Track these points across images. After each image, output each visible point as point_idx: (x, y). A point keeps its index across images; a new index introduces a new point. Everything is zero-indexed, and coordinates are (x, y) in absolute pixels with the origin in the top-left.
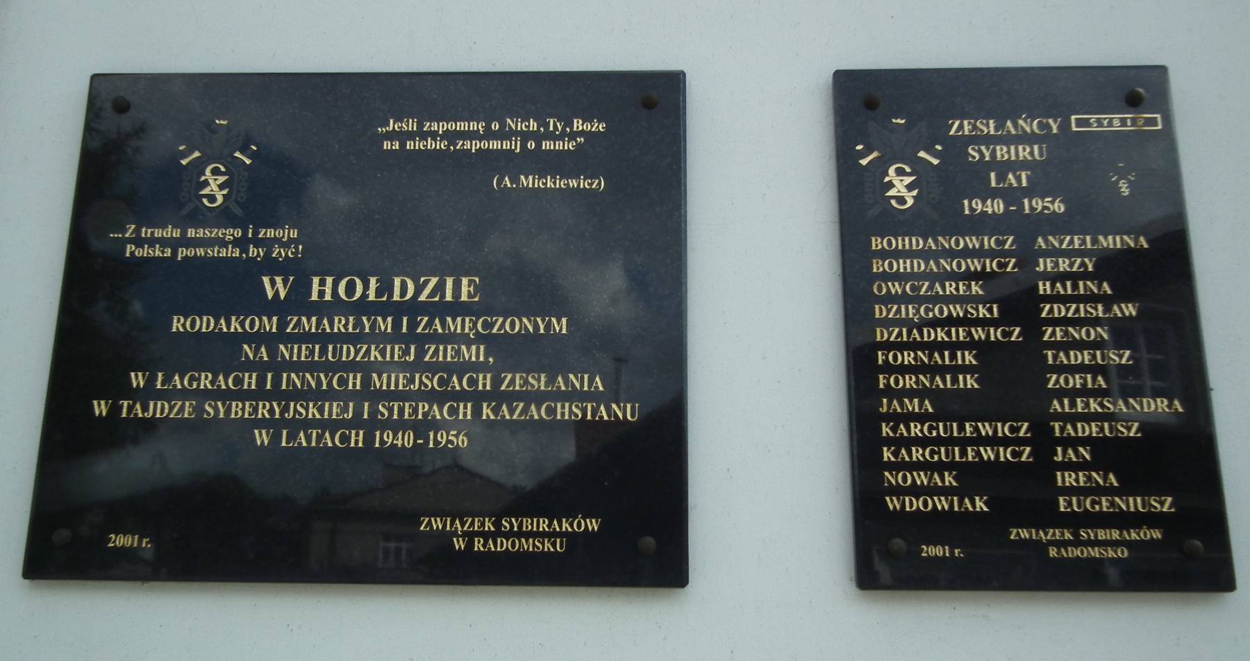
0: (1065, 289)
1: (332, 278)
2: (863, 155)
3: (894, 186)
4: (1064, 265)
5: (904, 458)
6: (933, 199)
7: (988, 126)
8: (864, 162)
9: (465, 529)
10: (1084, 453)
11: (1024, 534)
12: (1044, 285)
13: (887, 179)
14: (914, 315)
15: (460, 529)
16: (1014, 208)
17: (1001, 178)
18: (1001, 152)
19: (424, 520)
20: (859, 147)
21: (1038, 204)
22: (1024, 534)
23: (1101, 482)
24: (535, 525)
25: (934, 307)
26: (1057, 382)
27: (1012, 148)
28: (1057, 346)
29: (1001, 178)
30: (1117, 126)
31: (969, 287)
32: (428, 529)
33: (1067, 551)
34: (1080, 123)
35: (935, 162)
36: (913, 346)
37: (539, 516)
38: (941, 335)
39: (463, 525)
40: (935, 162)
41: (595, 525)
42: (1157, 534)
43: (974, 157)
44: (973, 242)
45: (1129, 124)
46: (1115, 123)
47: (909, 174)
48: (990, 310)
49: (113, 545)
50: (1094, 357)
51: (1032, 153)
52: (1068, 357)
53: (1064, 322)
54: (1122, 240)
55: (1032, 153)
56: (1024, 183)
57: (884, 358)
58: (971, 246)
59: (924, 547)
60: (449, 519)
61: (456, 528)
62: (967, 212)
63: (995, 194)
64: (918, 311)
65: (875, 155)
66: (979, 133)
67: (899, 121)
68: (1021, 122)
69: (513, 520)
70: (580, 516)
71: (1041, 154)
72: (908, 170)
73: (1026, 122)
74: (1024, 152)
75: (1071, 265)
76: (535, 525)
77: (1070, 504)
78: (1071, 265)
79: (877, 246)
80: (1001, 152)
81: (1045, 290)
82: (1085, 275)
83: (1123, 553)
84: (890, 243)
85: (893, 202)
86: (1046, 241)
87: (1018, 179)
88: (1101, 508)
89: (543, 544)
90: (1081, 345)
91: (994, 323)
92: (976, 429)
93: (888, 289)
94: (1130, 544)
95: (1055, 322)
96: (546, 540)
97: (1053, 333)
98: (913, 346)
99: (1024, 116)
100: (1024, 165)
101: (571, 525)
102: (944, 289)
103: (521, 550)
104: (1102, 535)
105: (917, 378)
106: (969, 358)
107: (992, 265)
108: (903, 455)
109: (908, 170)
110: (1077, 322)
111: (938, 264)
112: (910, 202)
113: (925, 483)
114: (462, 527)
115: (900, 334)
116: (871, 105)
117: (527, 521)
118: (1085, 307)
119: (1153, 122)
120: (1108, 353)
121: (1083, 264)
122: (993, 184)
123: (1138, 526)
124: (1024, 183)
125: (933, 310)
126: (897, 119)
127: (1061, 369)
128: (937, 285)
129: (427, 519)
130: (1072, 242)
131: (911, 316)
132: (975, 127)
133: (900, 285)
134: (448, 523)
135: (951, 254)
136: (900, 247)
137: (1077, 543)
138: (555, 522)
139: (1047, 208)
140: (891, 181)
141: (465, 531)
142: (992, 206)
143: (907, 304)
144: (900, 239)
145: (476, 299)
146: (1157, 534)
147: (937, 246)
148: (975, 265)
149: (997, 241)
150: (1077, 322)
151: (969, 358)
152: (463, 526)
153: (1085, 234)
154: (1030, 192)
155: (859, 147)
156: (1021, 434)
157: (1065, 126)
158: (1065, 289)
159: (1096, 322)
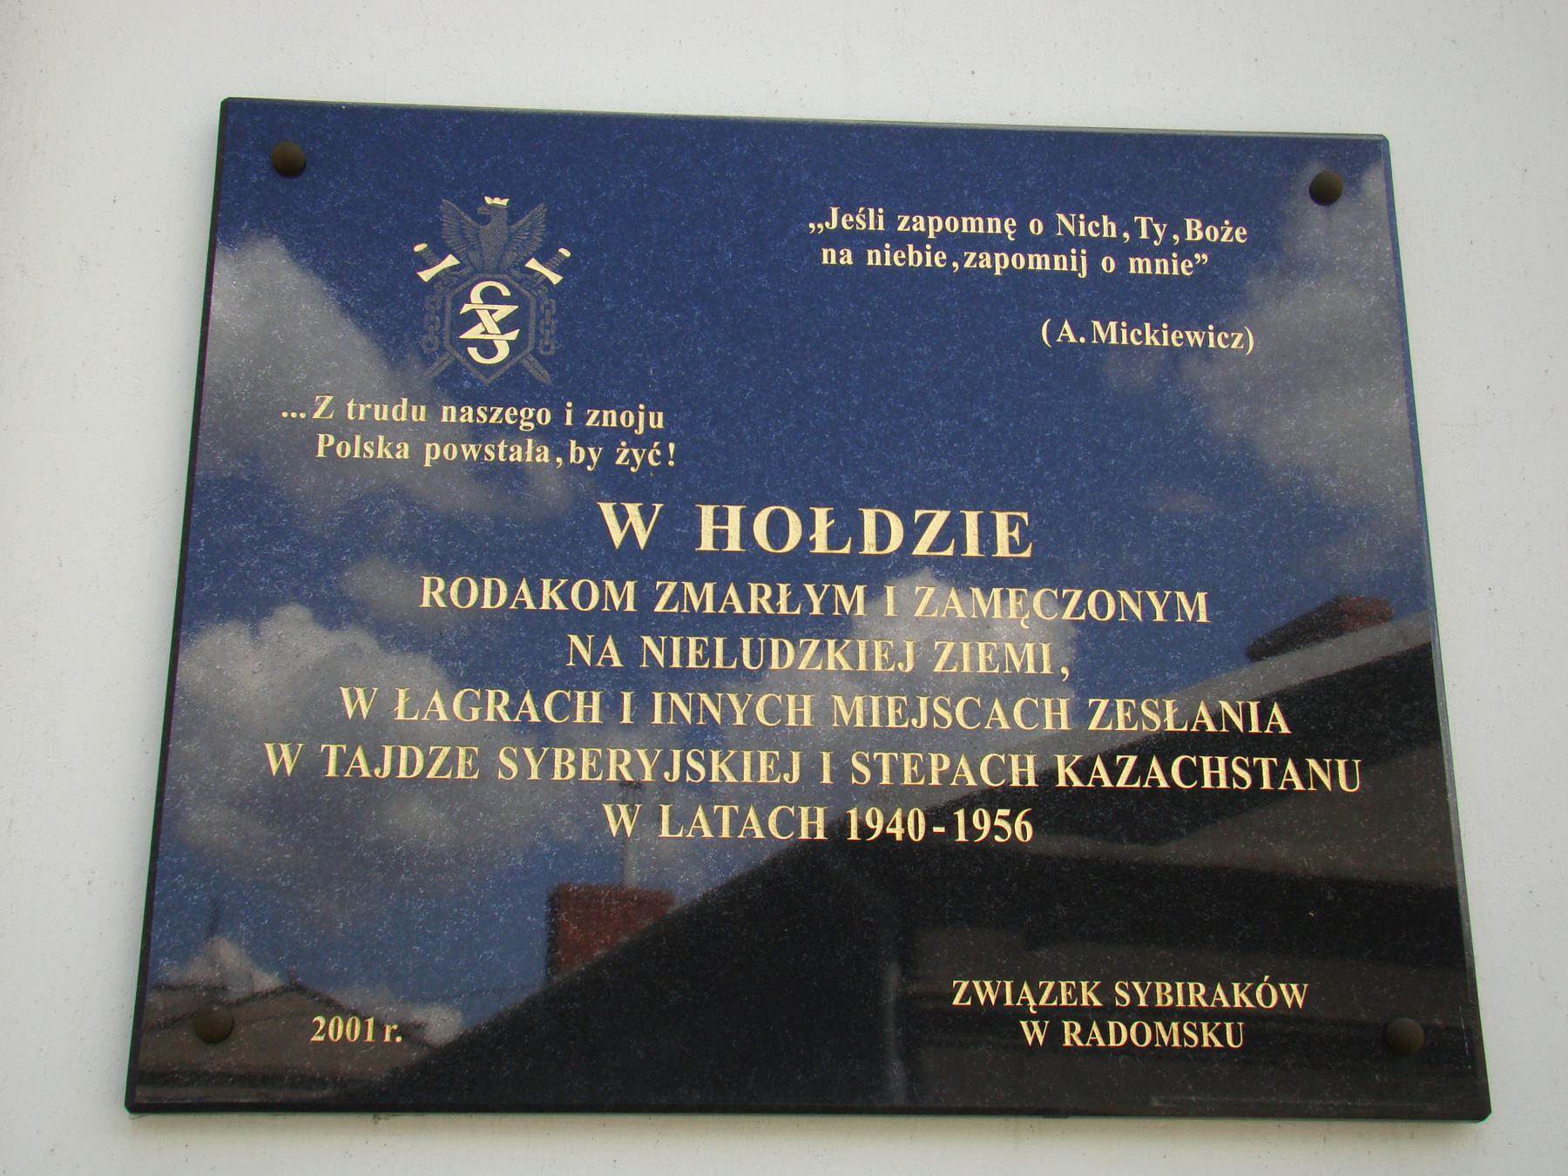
6: (547, 348)
9: (1042, 1002)
11: (986, 992)
15: (1032, 1003)
19: (959, 985)
35: (555, 279)
41: (1298, 996)
49: (321, 1038)
59: (321, 1020)
61: (1025, 1002)
67: (497, 201)
69: (1136, 985)
70: (1266, 977)
89: (1199, 1033)
96: (1205, 1025)
101: (1251, 994)
129: (965, 984)
138: (1219, 989)
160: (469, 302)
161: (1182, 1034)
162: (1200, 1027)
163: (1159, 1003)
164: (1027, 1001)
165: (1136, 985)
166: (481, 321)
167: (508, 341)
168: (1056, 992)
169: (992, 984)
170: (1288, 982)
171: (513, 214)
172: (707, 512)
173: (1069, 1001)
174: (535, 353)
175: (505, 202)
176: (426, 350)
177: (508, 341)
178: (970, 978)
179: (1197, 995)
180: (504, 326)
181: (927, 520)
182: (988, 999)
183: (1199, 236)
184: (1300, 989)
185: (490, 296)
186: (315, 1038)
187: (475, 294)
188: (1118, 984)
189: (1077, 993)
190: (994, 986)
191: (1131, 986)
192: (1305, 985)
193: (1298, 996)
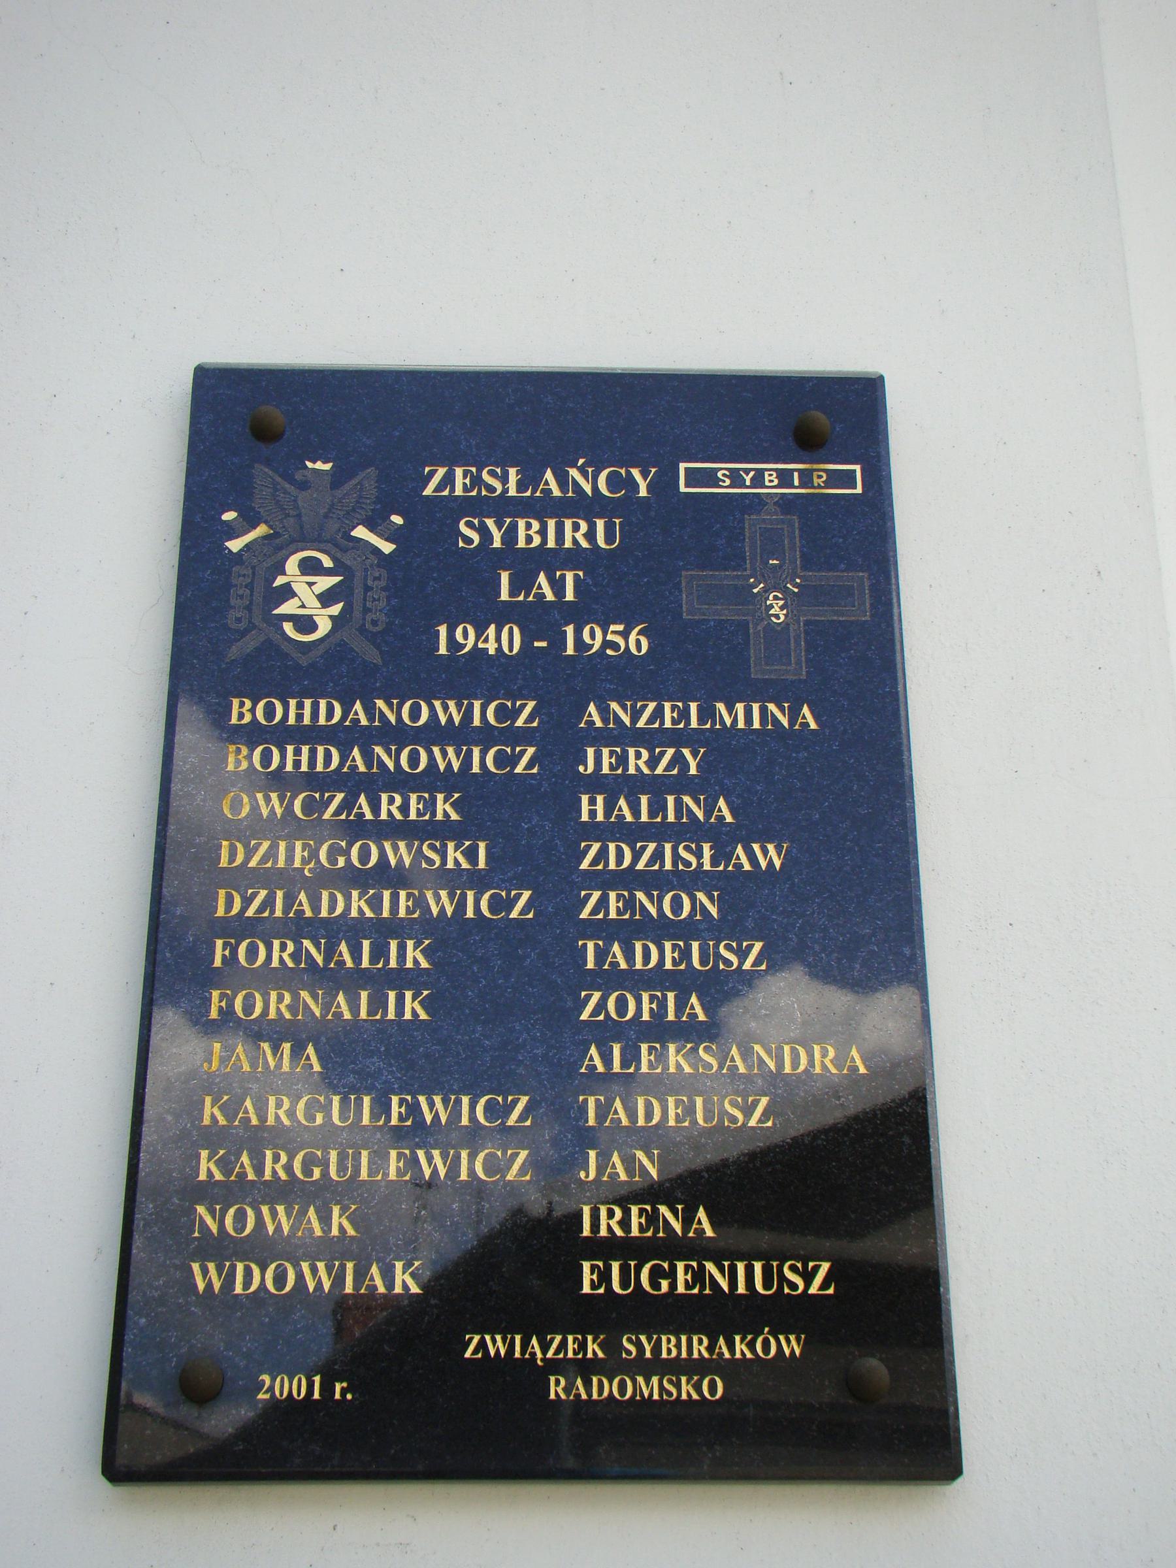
0: (636, 813)
1: (390, 891)
2: (232, 532)
3: (294, 595)
4: (637, 761)
5: (245, 1174)
6: (374, 623)
7: (504, 480)
8: (235, 545)
9: (550, 1355)
10: (646, 1162)
11: (497, 1346)
12: (592, 802)
13: (280, 581)
14: (305, 861)
15: (539, 1355)
16: (544, 644)
17: (522, 582)
18: (527, 533)
19: (471, 1339)
20: (229, 516)
21: (594, 636)
22: (497, 1346)
23: (677, 1227)
24: (684, 1349)
25: (350, 845)
26: (601, 1006)
27: (551, 524)
28: (605, 930)
29: (522, 582)
30: (771, 486)
31: (431, 805)
32: (480, 1355)
33: (588, 1384)
34: (694, 478)
35: (387, 548)
36: (298, 927)
37: (690, 1332)
38: (359, 905)
39: (545, 1348)
40: (387, 548)
41: (796, 1347)
42: (792, 1346)
43: (469, 541)
44: (449, 712)
45: (796, 483)
46: (767, 478)
47: (329, 572)
48: (471, 855)
49: (267, 1396)
50: (686, 954)
51: (591, 535)
52: (629, 955)
53: (627, 879)
54: (764, 711)
55: (591, 535)
56: (570, 596)
57: (227, 953)
58: (443, 719)
59: (266, 1378)
60: (518, 1338)
61: (533, 1354)
62: (443, 650)
63: (503, 615)
64: (314, 854)
65: (261, 530)
66: (484, 493)
67: (319, 465)
68: (574, 473)
69: (643, 1338)
70: (766, 1329)
71: (609, 538)
72: (327, 562)
73: (585, 474)
74: (575, 534)
75: (653, 762)
76: (684, 1349)
77: (604, 1277)
78: (653, 762)
79: (241, 716)
80: (527, 533)
81: (593, 813)
82: (681, 784)
83: (713, 1388)
84: (270, 712)
85: (288, 628)
86: (604, 711)
87: (558, 586)
88: (673, 1285)
89: (678, 1386)
90: (660, 929)
91: (479, 881)
92: (414, 1109)
93: (255, 808)
94: (730, 1370)
95: (606, 881)
96: (684, 1379)
97: (603, 903)
98: (298, 927)
99: (581, 461)
100: (574, 558)
101: (751, 1346)
102: (375, 808)
103: (638, 1398)
104: (670, 1347)
105: (296, 997)
106: (415, 956)
107: (483, 760)
108: (242, 1166)
109: (327, 562)
110: (655, 882)
111: (368, 756)
112: (324, 627)
113: (286, 1229)
114: (544, 1352)
115: (269, 903)
116: (264, 433)
117: (669, 1341)
118: (675, 850)
119: (847, 479)
120: (716, 946)
121: (678, 759)
122: (504, 596)
123: (751, 1329)
124: (570, 596)
125: (347, 853)
126: (314, 462)
127: (610, 979)
128: (362, 800)
129: (477, 1338)
130: (658, 713)
131: (297, 864)
132: (477, 481)
133: (281, 799)
134: (518, 1348)
135: (396, 736)
136: (292, 720)
137: (613, 1365)
138: (721, 1341)
139: (614, 646)
140: (288, 584)
141: (549, 1359)
142: (498, 639)
143: (291, 838)
144: (293, 703)
145: (416, 916)
146: (792, 1346)
147: (371, 719)
148: (449, 758)
149: (501, 712)
150: (655, 882)
151: (415, 956)
152: (545, 1350)
153: (686, 700)
154: (579, 614)
155: (229, 516)
156: (512, 1120)
157: (664, 485)
158: (636, 813)
159: (690, 880)
160: (284, 573)
161: (661, 1387)
162: (679, 1381)
163: (664, 1355)
164: (535, 1354)
165: (643, 1338)
166: (296, 595)
167: (330, 617)
168: (563, 1345)
169: (502, 1338)
170: (786, 1333)
171: (337, 479)
172: (585, 799)
173: (575, 1353)
174: (362, 630)
175: (327, 467)
176: (243, 626)
177: (330, 617)
178: (481, 1331)
179: (700, 1348)
180: (326, 599)
181: (644, 848)
182: (498, 1352)
183: (248, 718)
184: (798, 1340)
185: (310, 567)
186: (261, 1396)
187: (292, 565)
188: (625, 1337)
189: (583, 1346)
190: (504, 1340)
191: (638, 1339)
192: (803, 1336)
193: (796, 1347)
